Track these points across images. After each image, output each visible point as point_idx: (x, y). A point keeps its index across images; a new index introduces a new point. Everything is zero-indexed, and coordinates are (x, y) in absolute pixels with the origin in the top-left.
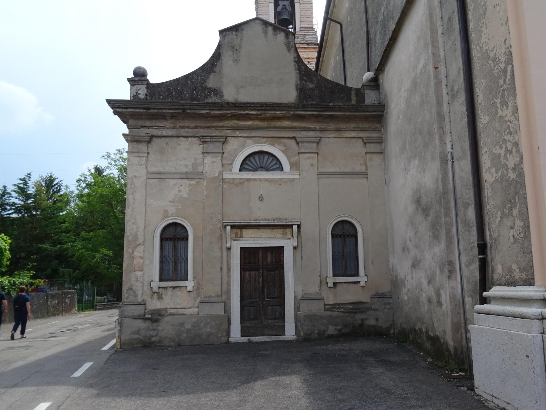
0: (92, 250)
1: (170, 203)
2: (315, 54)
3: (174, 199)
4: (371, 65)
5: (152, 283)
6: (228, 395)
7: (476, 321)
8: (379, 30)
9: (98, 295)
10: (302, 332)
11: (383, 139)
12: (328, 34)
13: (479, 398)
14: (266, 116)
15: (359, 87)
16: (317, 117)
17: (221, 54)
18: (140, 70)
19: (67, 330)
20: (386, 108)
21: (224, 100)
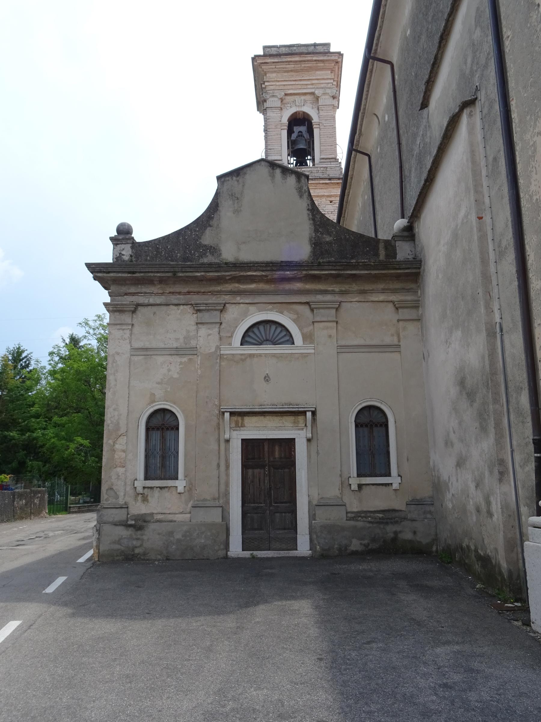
0: (66, 440)
1: (157, 385)
2: (338, 191)
3: (162, 379)
4: (406, 208)
5: (135, 482)
6: (223, 621)
7: (530, 537)
8: (414, 166)
9: (72, 494)
10: (318, 547)
11: (419, 302)
12: (354, 169)
13: (536, 635)
14: (273, 277)
15: (390, 238)
16: (336, 277)
17: (219, 205)
18: (124, 227)
19: (37, 537)
20: (423, 263)
21: (222, 259)
